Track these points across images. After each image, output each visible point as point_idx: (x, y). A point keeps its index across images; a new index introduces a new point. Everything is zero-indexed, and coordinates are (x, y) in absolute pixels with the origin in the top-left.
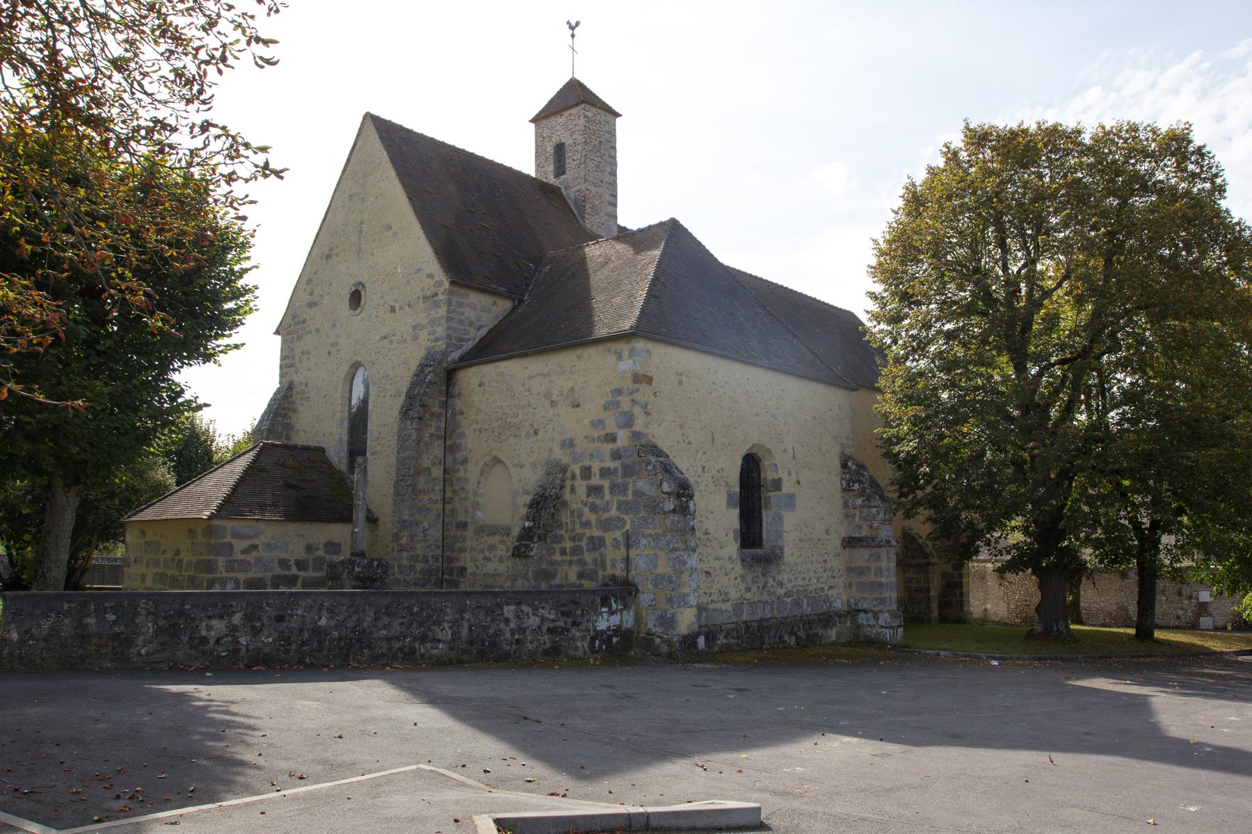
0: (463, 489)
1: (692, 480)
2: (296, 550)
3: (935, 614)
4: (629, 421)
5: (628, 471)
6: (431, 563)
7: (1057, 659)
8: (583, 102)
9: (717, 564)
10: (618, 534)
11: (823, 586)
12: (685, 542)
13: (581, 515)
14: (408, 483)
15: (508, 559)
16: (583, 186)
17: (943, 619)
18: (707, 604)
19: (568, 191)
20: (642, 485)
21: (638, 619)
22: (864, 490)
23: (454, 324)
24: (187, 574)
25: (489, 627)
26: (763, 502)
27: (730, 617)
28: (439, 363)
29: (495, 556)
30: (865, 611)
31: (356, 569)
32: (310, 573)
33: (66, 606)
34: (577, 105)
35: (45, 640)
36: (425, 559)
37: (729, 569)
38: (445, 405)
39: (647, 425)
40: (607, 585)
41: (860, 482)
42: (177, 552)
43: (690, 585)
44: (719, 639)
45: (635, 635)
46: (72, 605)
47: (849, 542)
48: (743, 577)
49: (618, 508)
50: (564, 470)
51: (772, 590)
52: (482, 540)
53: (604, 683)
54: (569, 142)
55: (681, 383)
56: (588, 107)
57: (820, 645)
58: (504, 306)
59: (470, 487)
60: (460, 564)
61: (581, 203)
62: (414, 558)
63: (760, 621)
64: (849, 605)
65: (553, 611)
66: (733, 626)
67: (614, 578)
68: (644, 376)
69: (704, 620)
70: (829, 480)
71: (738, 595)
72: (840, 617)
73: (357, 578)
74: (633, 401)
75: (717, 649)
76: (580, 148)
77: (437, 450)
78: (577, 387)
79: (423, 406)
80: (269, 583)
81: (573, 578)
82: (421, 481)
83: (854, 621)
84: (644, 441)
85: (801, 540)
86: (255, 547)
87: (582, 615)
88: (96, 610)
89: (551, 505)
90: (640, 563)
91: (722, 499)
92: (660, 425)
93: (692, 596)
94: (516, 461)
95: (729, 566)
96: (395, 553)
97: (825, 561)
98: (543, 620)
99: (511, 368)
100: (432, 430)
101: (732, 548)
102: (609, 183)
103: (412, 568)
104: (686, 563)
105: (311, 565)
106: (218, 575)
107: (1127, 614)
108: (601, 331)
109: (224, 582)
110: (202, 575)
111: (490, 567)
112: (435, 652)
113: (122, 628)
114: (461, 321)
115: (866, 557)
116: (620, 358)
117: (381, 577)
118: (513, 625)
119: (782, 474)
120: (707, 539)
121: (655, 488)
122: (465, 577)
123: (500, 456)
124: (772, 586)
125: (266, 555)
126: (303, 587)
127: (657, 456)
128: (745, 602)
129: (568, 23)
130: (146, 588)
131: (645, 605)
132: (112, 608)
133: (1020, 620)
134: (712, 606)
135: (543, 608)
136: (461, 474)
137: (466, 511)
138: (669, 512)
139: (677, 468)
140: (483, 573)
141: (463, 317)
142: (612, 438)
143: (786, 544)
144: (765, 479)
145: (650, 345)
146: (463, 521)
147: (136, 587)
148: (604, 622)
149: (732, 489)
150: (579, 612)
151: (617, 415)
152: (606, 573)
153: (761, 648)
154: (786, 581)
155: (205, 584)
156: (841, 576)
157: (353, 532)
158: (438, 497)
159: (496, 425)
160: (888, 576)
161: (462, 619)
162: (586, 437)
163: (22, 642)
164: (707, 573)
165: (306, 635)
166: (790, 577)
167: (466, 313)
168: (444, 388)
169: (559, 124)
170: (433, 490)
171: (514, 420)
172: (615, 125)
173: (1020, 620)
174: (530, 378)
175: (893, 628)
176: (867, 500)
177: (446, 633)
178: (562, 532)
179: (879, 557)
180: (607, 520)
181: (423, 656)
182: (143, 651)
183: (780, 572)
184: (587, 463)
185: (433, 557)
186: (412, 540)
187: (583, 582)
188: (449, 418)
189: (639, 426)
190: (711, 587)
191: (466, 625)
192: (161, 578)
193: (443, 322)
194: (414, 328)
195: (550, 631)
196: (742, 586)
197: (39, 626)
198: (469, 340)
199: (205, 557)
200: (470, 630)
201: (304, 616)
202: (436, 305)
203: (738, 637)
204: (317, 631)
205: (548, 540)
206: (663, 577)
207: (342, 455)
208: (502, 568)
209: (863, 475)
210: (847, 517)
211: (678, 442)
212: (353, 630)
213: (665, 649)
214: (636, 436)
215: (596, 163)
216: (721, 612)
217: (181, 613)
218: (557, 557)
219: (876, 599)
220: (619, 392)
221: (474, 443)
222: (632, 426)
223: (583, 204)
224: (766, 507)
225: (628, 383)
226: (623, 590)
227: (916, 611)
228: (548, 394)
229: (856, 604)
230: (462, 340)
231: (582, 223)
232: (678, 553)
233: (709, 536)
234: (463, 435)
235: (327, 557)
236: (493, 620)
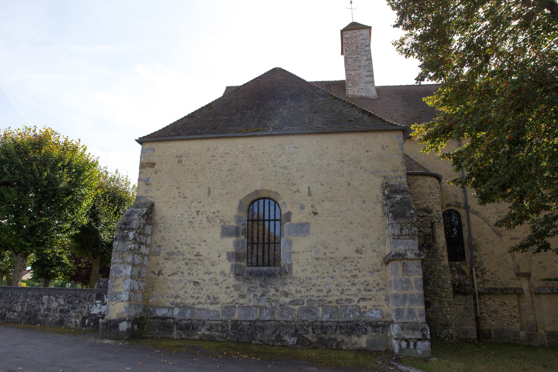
31: (101, 283)
44: (200, 330)
48: (236, 287)
51: (273, 298)
63: (252, 323)
66: (220, 322)
69: (188, 316)
75: (197, 337)
85: (317, 259)
93: (123, 294)
95: (220, 278)
98: (60, 305)
104: (121, 272)
128: (237, 306)
143: (294, 262)
164: (196, 283)
166: (299, 288)
191: (26, 304)
195: (61, 311)
200: (28, 307)
203: (223, 332)
216: (208, 311)
233: (201, 258)
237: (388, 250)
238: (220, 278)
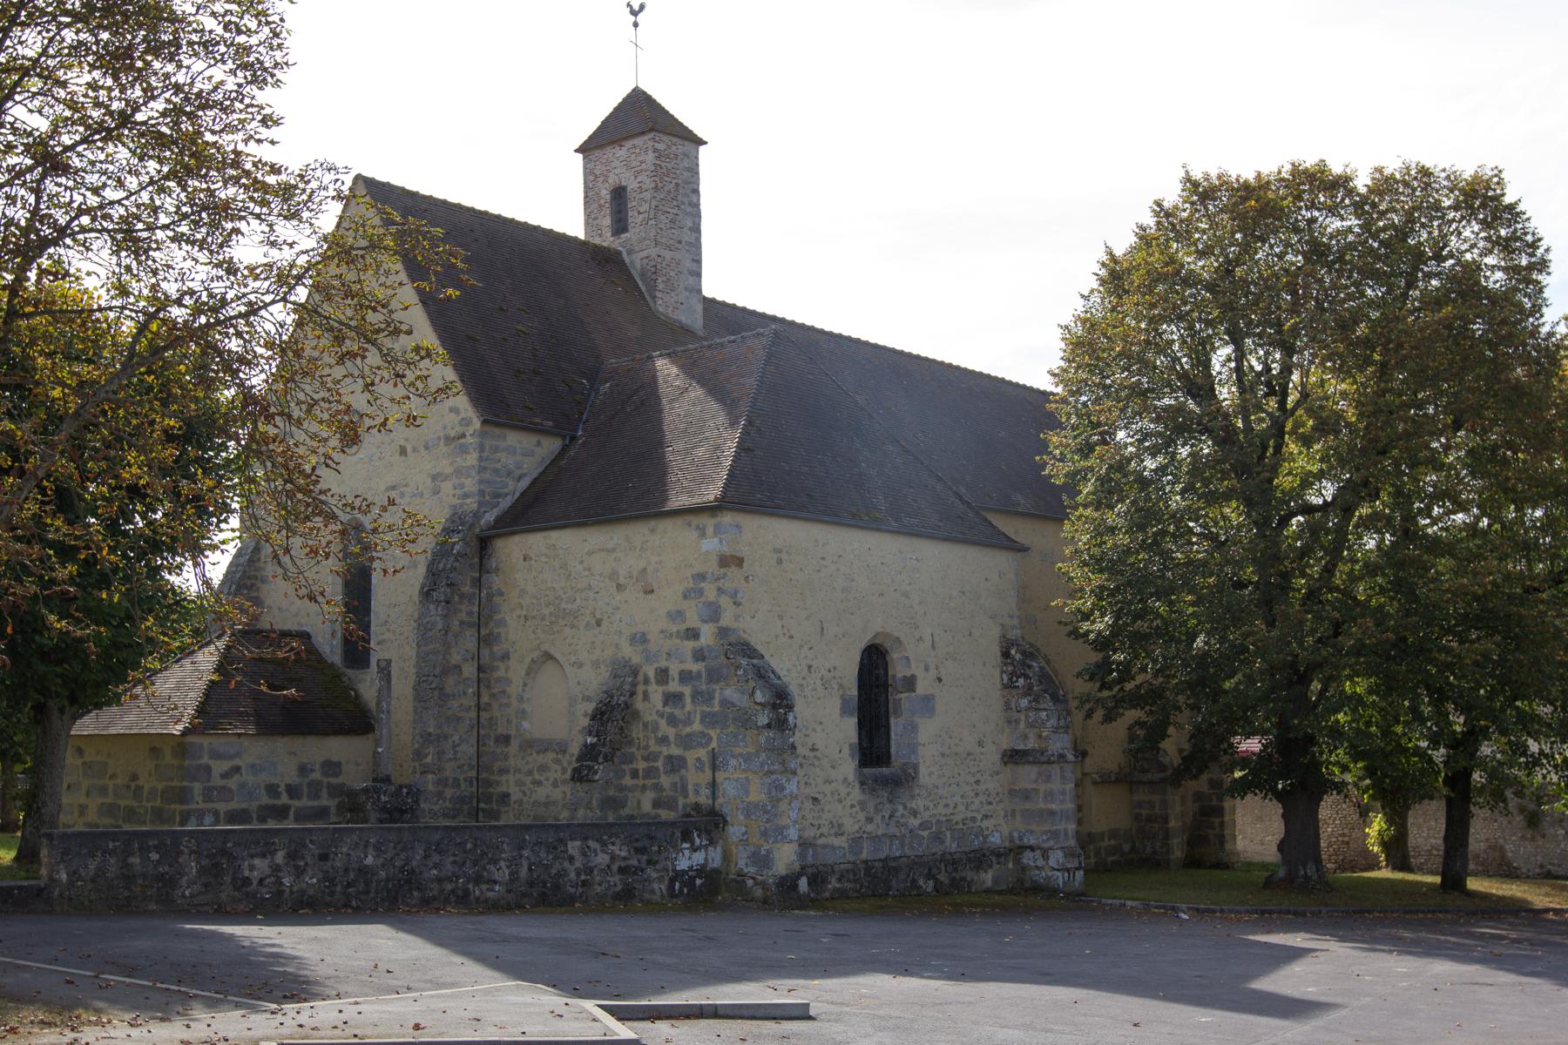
0: (504, 692)
1: (793, 689)
2: (287, 773)
3: (1178, 854)
4: (714, 614)
5: (714, 676)
6: (463, 787)
7: (1288, 912)
8: (652, 130)
9: (828, 789)
10: (702, 753)
11: (974, 814)
12: (783, 763)
13: (656, 728)
14: (434, 685)
15: (564, 782)
16: (653, 252)
17: (1193, 862)
18: (815, 838)
19: (634, 256)
20: (731, 693)
21: (726, 857)
22: (1030, 688)
23: (487, 476)
24: (150, 804)
25: (551, 866)
26: (891, 706)
27: (844, 855)
28: (469, 529)
29: (547, 779)
30: (1032, 849)
31: (382, 797)
32: (305, 802)
33: (111, 845)
34: (643, 133)
35: (93, 881)
36: (456, 781)
37: (843, 794)
38: (478, 583)
39: (737, 618)
40: (688, 815)
41: (1026, 676)
42: (134, 777)
43: (789, 816)
45: (723, 876)
46: (117, 844)
47: (1011, 756)
48: (862, 804)
49: (702, 721)
50: (635, 672)
51: (902, 821)
52: (530, 759)
53: (685, 927)
54: (632, 185)
55: (780, 562)
56: (659, 136)
57: (969, 892)
58: (552, 445)
59: (514, 689)
60: (502, 789)
61: (651, 275)
62: (442, 782)
63: (885, 860)
64: (1012, 841)
65: (625, 848)
66: (849, 866)
67: (697, 807)
68: (733, 557)
70: (986, 675)
71: (856, 827)
72: (999, 855)
73: (384, 809)
74: (719, 589)
75: (827, 894)
76: (647, 195)
77: (469, 641)
78: (650, 569)
79: (450, 585)
80: (255, 816)
81: (647, 807)
82: (450, 682)
83: (1017, 861)
84: (732, 639)
85: (943, 755)
86: (237, 769)
87: (659, 852)
88: (140, 849)
89: (619, 717)
90: (729, 788)
91: (834, 705)
92: (753, 617)
94: (574, 659)
95: (843, 790)
96: (418, 775)
97: (977, 782)
98: (613, 857)
99: (565, 540)
100: (463, 616)
101: (848, 767)
102: (690, 244)
103: (440, 794)
105: (305, 790)
106: (194, 806)
107: (1503, 856)
108: (677, 501)
109: (201, 815)
110: (173, 806)
111: (541, 793)
112: (490, 894)
113: (167, 868)
114: (496, 471)
115: (1033, 776)
116: (703, 534)
117: (411, 808)
118: (578, 864)
119: (916, 669)
120: (815, 757)
121: (746, 697)
122: (508, 805)
123: (552, 651)
124: (903, 816)
125: (250, 779)
126: (297, 820)
127: (749, 657)
129: (629, 5)
130: (87, 824)
131: (735, 839)
132: (156, 847)
133: (1334, 866)
134: (821, 841)
135: (613, 844)
136: (501, 673)
137: (509, 721)
138: (763, 727)
139: (773, 672)
140: (532, 800)
141: (498, 466)
142: (693, 634)
144: (894, 676)
145: (741, 519)
146: (505, 733)
147: (71, 823)
148: (686, 860)
149: (848, 692)
150: (655, 848)
151: (700, 605)
152: (687, 800)
153: (887, 895)
154: (922, 809)
155: (178, 818)
156: (1001, 801)
157: (375, 753)
158: (473, 703)
159: (546, 612)
160: (1062, 802)
161: (521, 857)
162: (662, 632)
163: (71, 883)
164: (815, 799)
165: (352, 875)
167: (503, 460)
168: (477, 560)
169: (617, 158)
170: (464, 693)
171: (570, 606)
172: (697, 158)
173: (1334, 866)
174: (590, 553)
175: (1068, 870)
176: (1035, 700)
177: (502, 873)
178: (634, 750)
179: (1050, 777)
180: (688, 735)
181: (477, 899)
182: (187, 893)
183: (913, 797)
184: (663, 664)
185: (465, 780)
186: (439, 759)
187: (660, 811)
188: (484, 601)
189: (726, 620)
190: (820, 817)
191: (525, 863)
192: (110, 810)
193: (474, 473)
194: (434, 478)
195: (622, 870)
196: (861, 816)
197: (86, 866)
198: (506, 495)
199: (176, 783)
200: (530, 869)
201: (348, 855)
202: (464, 450)
203: (855, 881)
204: (363, 871)
205: (616, 759)
206: (756, 805)
207: (335, 643)
208: (557, 794)
209: (1030, 667)
210: (1009, 722)
211: (777, 637)
212: (402, 870)
213: (758, 892)
214: (723, 632)
215: (670, 216)
216: (833, 848)
217: (224, 852)
218: (628, 781)
219: (1045, 833)
220: (701, 577)
221: (518, 635)
222: (718, 620)
223: (654, 277)
224: (895, 713)
225: (712, 567)
226: (709, 822)
227: (1149, 850)
228: (613, 575)
229: (1021, 839)
230: (497, 496)
231: (652, 304)
232: (774, 777)
233: (818, 753)
234: (502, 623)
235: (325, 780)
236: (556, 858)
237: (1006, 742)
238: (843, 790)
